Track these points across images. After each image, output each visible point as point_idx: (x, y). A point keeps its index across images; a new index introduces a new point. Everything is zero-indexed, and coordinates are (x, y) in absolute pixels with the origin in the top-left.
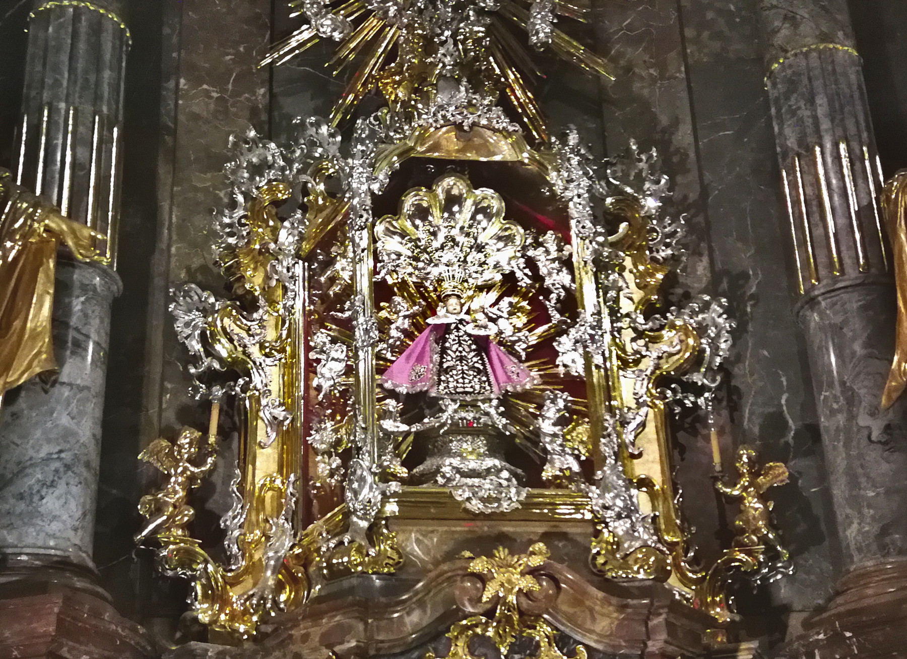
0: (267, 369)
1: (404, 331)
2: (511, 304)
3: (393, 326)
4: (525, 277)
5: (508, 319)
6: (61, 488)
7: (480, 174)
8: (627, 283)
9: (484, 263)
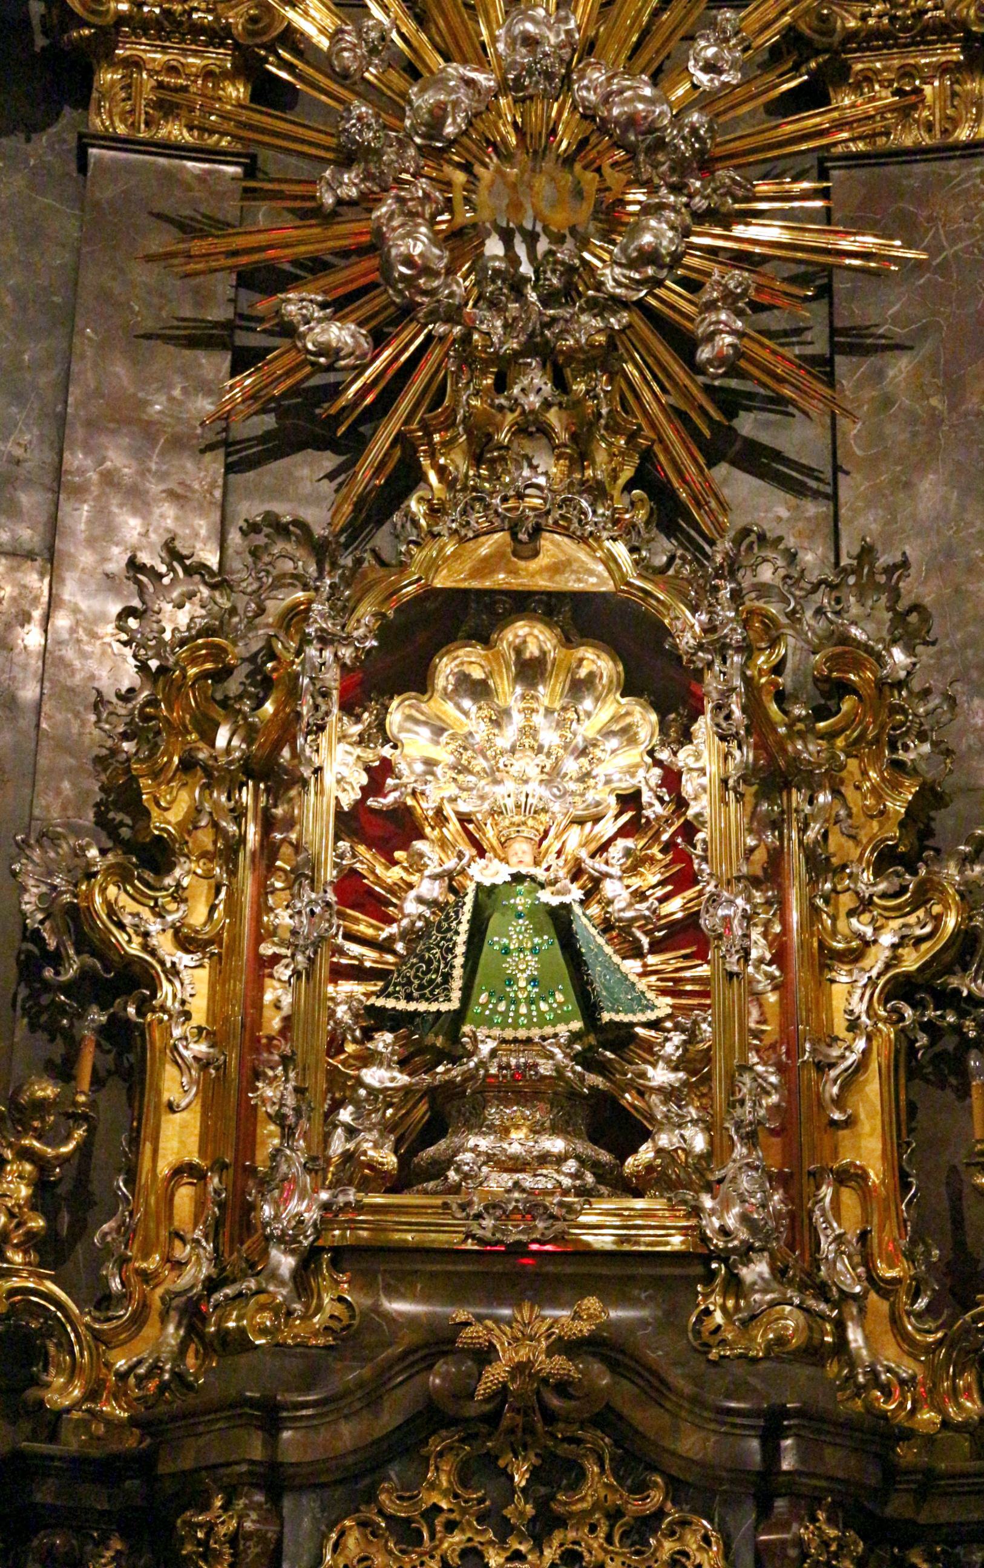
0: (185, 975)
1: (433, 904)
3: (412, 894)
4: (656, 803)
5: (620, 878)
7: (581, 617)
8: (849, 809)
9: (588, 774)
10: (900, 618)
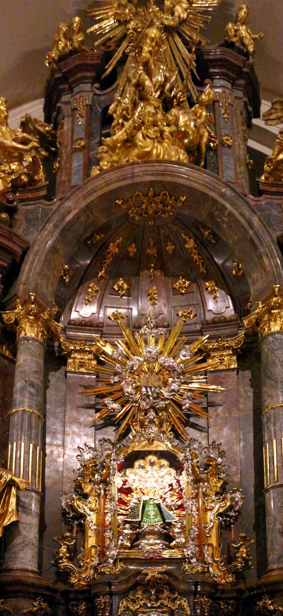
2: (170, 494)
6: (25, 551)
7: (162, 455)
10: (220, 453)
